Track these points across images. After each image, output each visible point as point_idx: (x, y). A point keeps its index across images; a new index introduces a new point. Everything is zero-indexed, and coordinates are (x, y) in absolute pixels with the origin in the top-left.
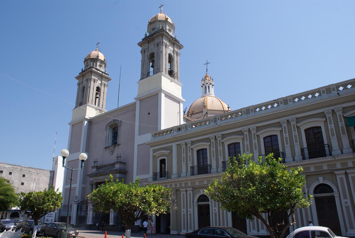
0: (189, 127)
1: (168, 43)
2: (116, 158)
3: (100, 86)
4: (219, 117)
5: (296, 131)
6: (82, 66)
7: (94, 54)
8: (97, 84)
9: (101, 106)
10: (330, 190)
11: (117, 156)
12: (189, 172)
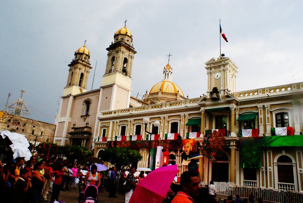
3: (84, 73)
6: (73, 57)
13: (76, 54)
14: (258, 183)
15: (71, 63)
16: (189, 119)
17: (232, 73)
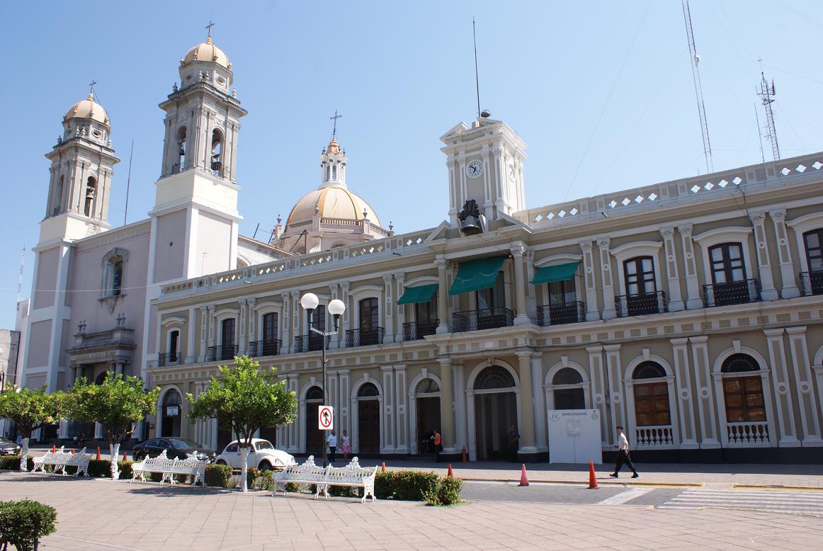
0: (400, 245)
1: (213, 110)
2: (117, 321)
3: (95, 175)
4: (255, 269)
5: (784, 237)
6: (60, 131)
7: (83, 107)
8: (90, 171)
9: (97, 215)
10: (659, 371)
11: (118, 317)
12: (399, 332)
13: (67, 121)
14: (675, 432)
15: (53, 150)
17: (511, 161)
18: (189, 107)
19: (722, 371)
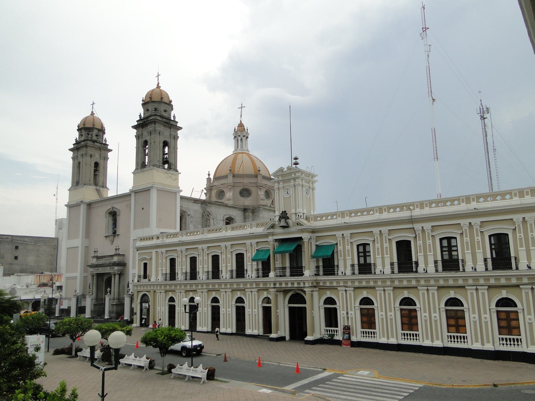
16: (257, 250)
18: (149, 130)
19: (496, 307)
